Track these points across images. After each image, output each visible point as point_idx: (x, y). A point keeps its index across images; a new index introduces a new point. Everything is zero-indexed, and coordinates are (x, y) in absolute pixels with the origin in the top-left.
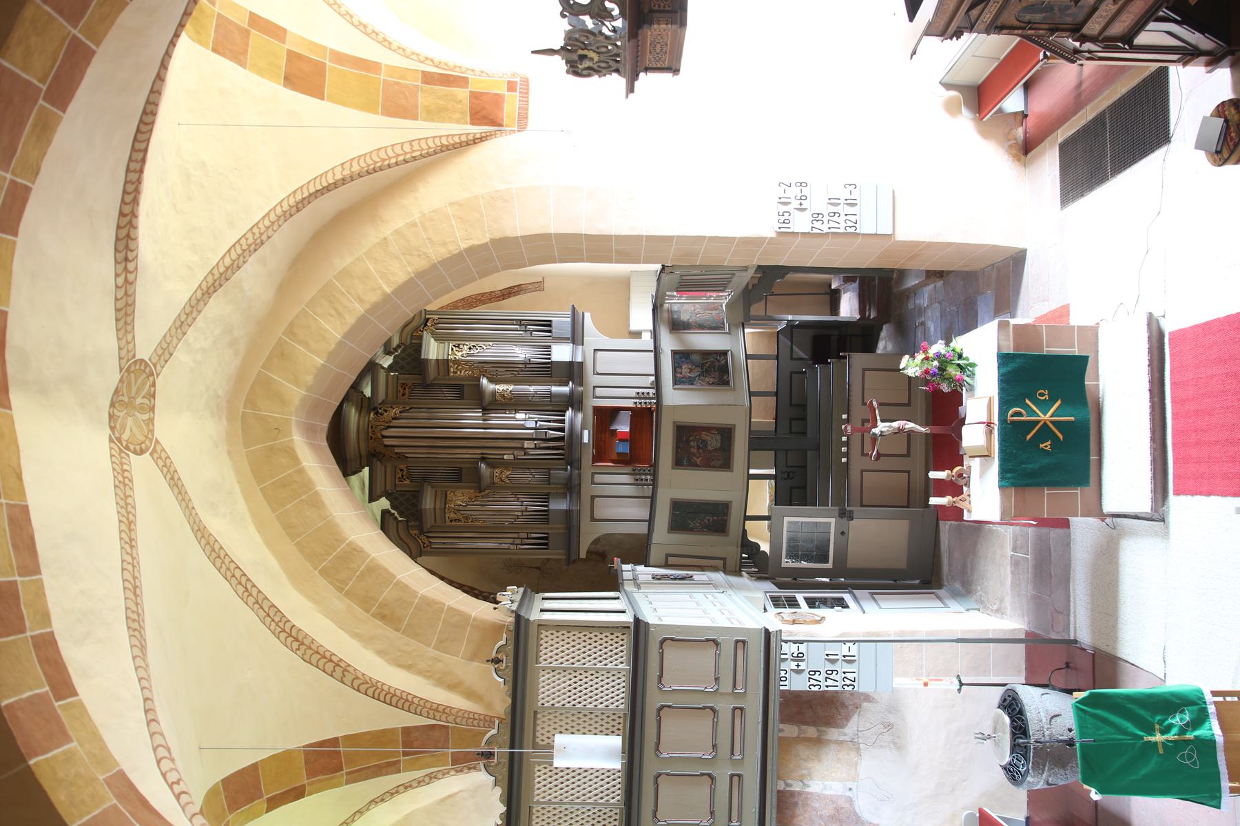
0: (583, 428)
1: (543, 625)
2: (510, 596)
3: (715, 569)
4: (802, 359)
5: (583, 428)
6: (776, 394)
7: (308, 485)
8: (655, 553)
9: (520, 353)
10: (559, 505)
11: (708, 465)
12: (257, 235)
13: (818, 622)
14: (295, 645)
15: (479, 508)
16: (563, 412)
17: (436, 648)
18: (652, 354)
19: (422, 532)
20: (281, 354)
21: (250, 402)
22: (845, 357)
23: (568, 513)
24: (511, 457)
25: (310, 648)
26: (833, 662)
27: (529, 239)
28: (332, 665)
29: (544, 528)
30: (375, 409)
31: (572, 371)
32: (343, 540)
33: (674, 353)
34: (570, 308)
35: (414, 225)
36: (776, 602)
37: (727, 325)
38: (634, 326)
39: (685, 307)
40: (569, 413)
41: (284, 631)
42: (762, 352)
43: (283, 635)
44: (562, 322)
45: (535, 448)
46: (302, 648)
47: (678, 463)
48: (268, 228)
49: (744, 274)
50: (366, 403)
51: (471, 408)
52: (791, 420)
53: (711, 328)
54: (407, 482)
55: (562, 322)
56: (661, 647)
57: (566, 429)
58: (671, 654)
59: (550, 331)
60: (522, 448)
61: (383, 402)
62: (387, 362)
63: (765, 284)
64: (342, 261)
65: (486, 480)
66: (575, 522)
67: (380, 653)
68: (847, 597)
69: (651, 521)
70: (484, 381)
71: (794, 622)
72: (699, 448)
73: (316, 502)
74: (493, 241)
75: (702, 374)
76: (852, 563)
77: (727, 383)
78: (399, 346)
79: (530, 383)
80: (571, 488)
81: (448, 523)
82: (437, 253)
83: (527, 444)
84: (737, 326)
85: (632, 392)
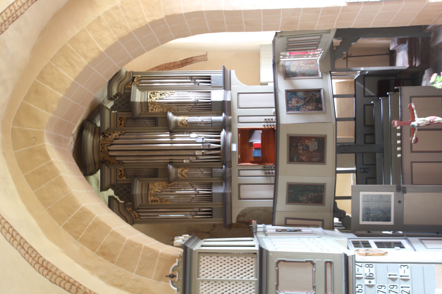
0: (232, 142)
1: (201, 253)
2: (180, 240)
3: (316, 226)
4: (371, 96)
5: (232, 142)
6: (355, 119)
7: (55, 172)
8: (278, 218)
9: (192, 97)
10: (218, 190)
11: (310, 161)
12: (13, 11)
13: (383, 255)
14: (45, 272)
15: (169, 193)
16: (219, 132)
17: (137, 273)
18: (273, 95)
19: (134, 209)
20: (36, 91)
21: (17, 121)
22: (397, 90)
23: (224, 195)
24: (188, 161)
25: (55, 274)
26: (394, 280)
27: (189, 15)
28: (69, 284)
29: (209, 204)
30: (103, 133)
31: (224, 107)
32: (78, 206)
33: (287, 91)
34: (222, 68)
35: (117, 8)
36: (356, 244)
37: (320, 73)
38: (263, 80)
39: (294, 62)
40: (223, 133)
41: (38, 263)
42: (346, 93)
43: (37, 266)
44: (217, 76)
45: (203, 155)
46: (50, 274)
47: (291, 160)
48: (20, 7)
49: (328, 35)
50: (97, 131)
51: (164, 131)
52: (365, 135)
53: (310, 75)
54: (124, 178)
55: (217, 76)
56: (277, 266)
57: (222, 143)
58: (284, 270)
59: (210, 83)
60: (194, 155)
61: (108, 129)
62: (110, 105)
63: (345, 45)
64: (72, 32)
65: (173, 176)
66: (228, 201)
67: (102, 277)
68: (404, 242)
69: (275, 199)
70: (170, 115)
71: (366, 255)
72: (304, 150)
73: (61, 183)
74: (167, 17)
75: (305, 104)
76: (407, 221)
77: (321, 109)
78: (117, 95)
79: (199, 115)
80: (225, 179)
81: (150, 203)
82: (132, 26)
83: (197, 153)
84: (327, 73)
85: (262, 119)
